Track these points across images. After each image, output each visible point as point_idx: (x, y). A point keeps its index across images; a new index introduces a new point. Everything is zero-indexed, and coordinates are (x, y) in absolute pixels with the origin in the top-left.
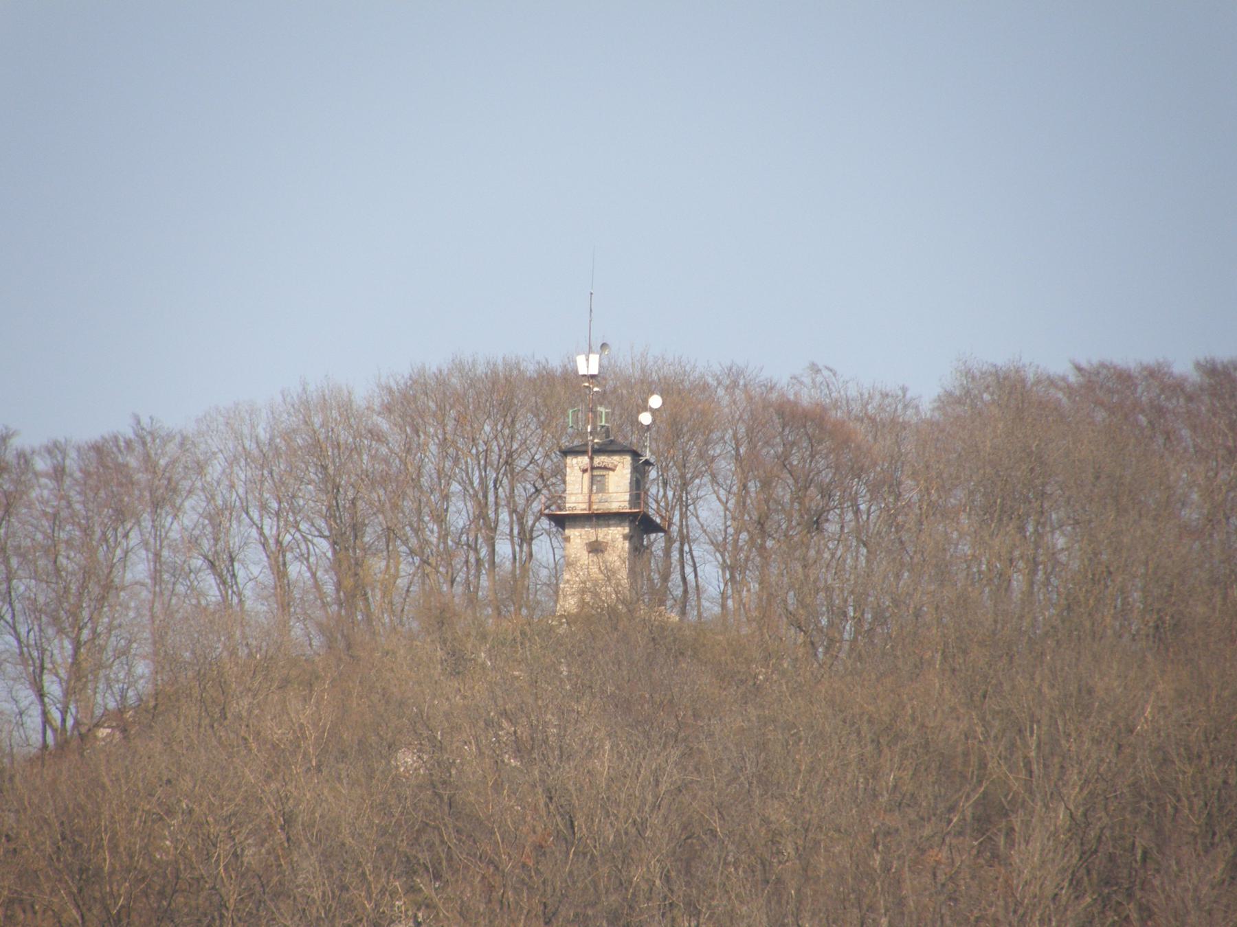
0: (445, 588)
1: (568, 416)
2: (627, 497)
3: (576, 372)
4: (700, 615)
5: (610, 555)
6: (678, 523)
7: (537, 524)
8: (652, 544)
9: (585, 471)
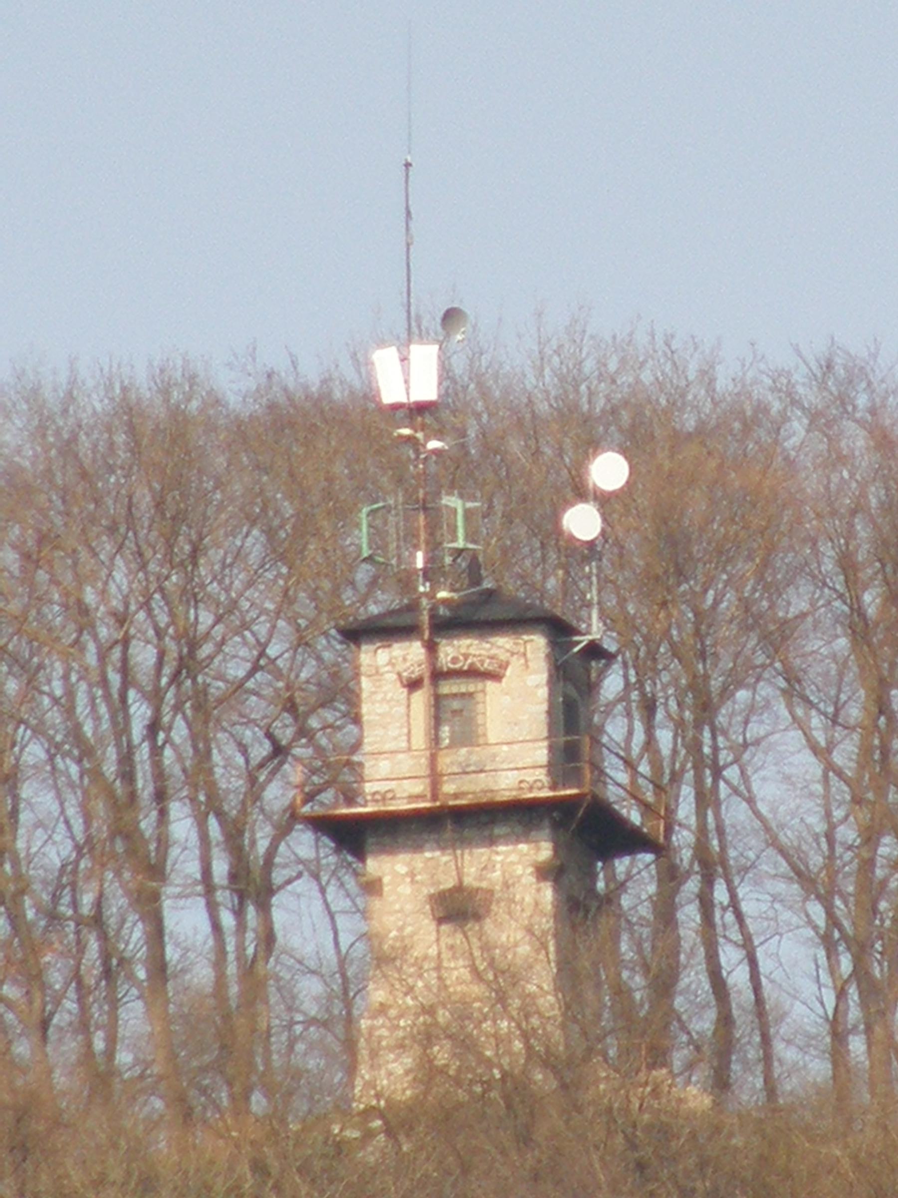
0: (22, 1049)
1: (358, 525)
2: (541, 754)
3: (371, 395)
4: (771, 1088)
5: (499, 925)
6: (693, 821)
7: (282, 848)
8: (622, 886)
9: (413, 685)
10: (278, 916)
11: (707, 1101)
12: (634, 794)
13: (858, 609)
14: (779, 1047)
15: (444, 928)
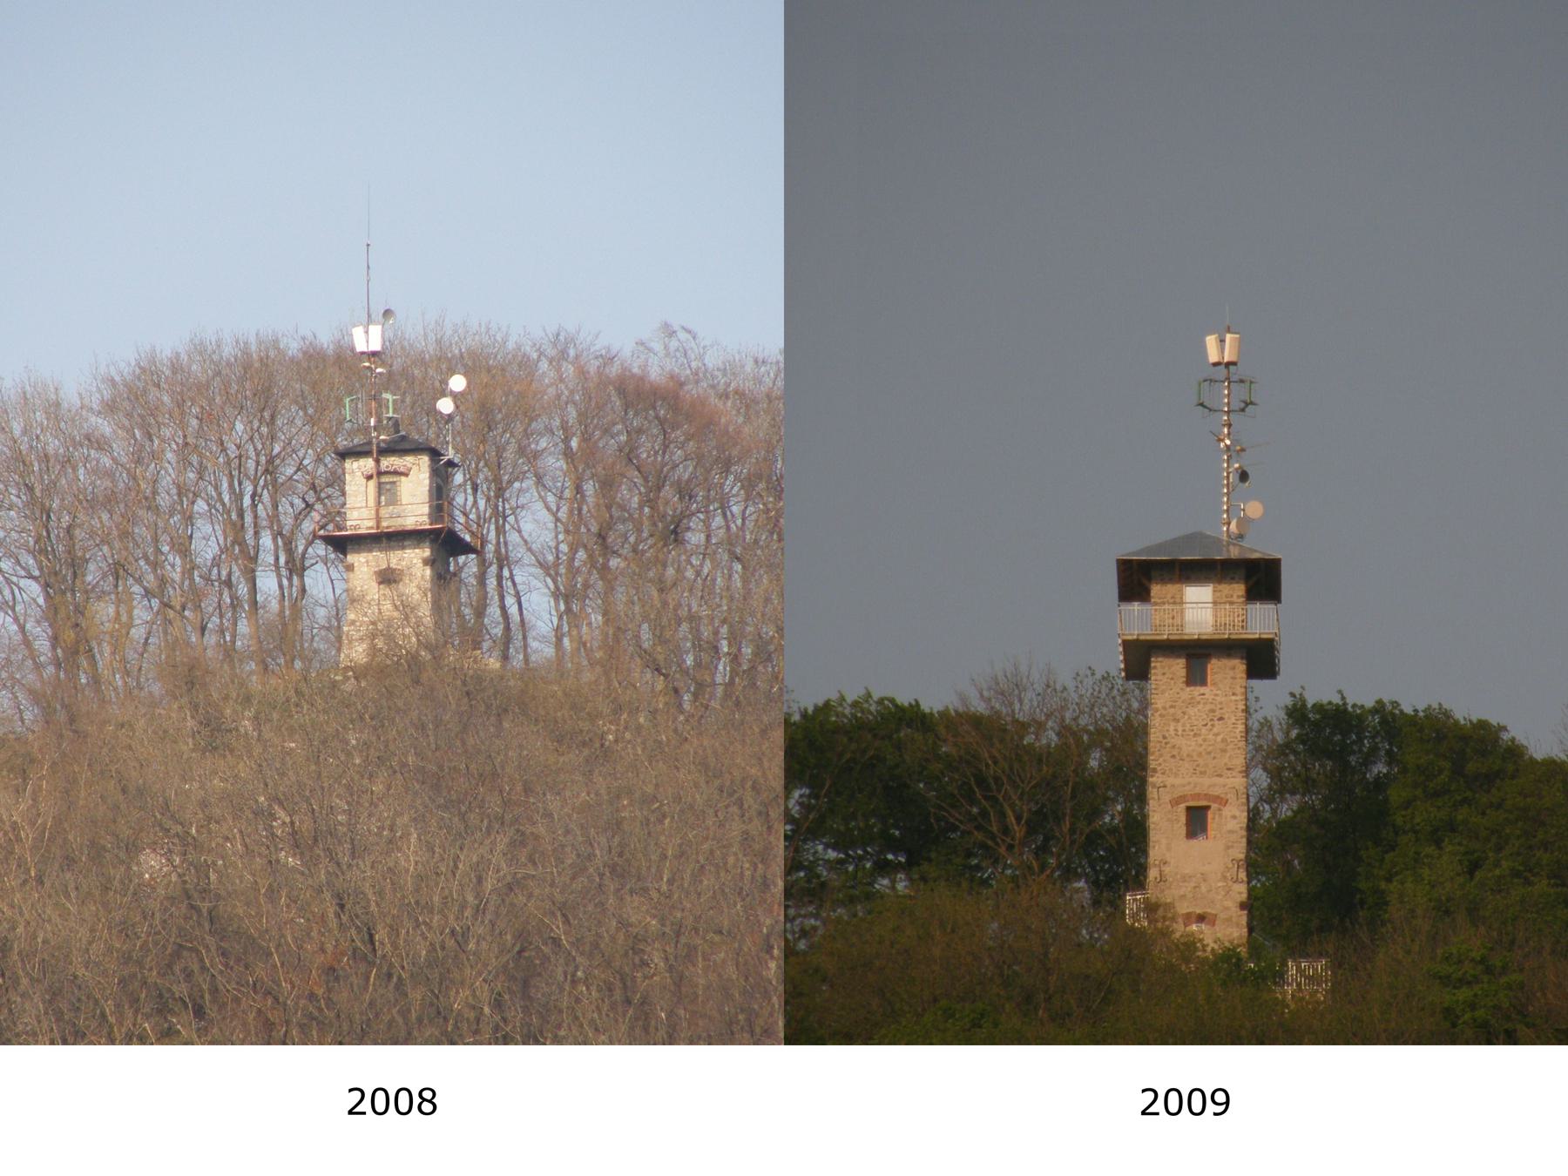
1: (344, 407)
2: (426, 509)
3: (353, 349)
4: (526, 660)
10: (307, 581)
11: (498, 665)
12: (467, 528)
13: (568, 447)
14: (530, 641)
15: (381, 586)
